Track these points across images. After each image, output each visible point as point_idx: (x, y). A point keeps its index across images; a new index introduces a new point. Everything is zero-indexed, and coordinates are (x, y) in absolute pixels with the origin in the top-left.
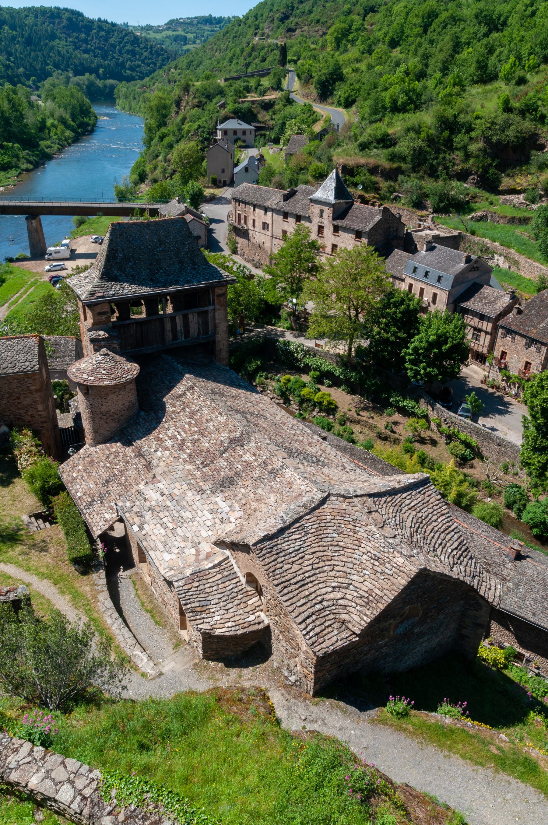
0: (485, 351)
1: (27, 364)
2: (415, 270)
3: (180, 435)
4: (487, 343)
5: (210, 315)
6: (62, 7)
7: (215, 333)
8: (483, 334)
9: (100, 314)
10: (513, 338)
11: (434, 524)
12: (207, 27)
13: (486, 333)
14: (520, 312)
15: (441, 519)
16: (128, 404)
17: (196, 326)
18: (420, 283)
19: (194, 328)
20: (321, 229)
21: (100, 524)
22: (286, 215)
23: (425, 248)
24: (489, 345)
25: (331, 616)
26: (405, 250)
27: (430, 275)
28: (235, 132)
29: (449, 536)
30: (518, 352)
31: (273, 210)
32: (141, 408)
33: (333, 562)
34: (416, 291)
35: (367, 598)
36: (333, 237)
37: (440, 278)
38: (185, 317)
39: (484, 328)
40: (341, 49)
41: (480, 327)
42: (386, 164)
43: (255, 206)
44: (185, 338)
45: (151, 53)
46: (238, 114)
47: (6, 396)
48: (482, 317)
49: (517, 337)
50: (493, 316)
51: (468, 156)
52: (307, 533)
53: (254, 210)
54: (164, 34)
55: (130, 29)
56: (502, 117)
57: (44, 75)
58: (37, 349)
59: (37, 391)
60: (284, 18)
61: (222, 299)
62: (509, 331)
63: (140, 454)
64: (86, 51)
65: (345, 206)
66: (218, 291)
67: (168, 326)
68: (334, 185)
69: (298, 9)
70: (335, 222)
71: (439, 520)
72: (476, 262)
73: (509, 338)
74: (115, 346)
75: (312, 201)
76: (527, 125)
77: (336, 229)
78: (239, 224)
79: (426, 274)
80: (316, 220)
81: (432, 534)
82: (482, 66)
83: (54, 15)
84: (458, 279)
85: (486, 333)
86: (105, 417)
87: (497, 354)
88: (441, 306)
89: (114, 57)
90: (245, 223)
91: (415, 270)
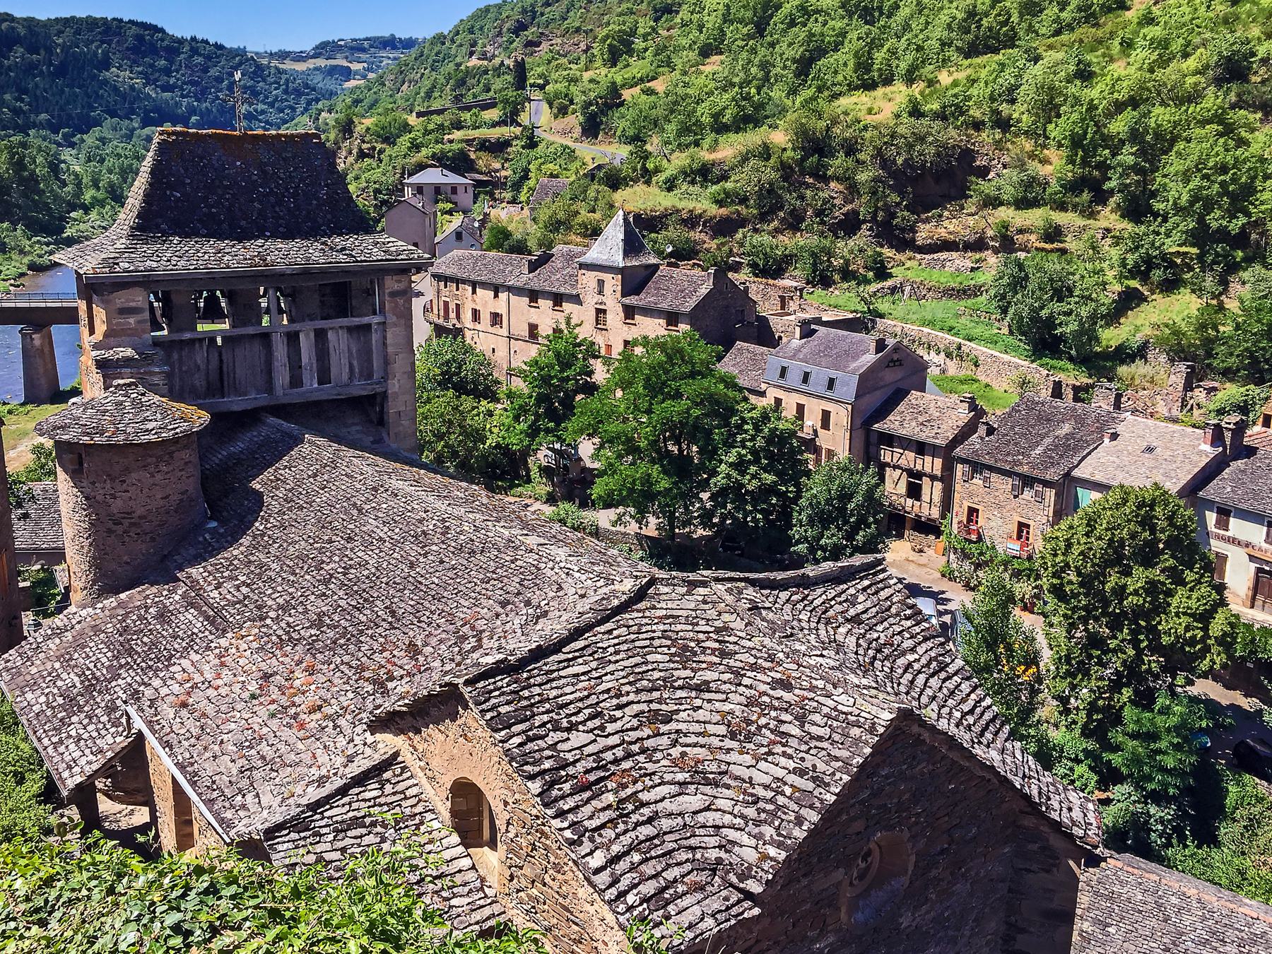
0: (935, 513)
5: (375, 337)
6: (126, 19)
7: (385, 378)
11: (911, 657)
13: (933, 478)
14: (991, 430)
15: (924, 646)
17: (345, 361)
18: (794, 395)
19: (340, 367)
20: (601, 313)
21: (83, 761)
22: (534, 296)
23: (798, 335)
24: (942, 502)
25: (683, 856)
28: (437, 189)
29: (950, 684)
31: (510, 289)
33: (673, 726)
34: (789, 412)
35: (771, 801)
36: (626, 328)
37: (831, 383)
38: (320, 335)
39: (928, 469)
40: (620, 65)
41: (919, 467)
42: (713, 210)
43: (474, 285)
45: (286, 92)
46: (441, 161)
48: (921, 448)
49: (995, 477)
51: (853, 189)
52: (603, 662)
53: (474, 292)
54: (311, 64)
55: (249, 55)
56: (906, 127)
57: (86, 125)
60: (520, 28)
62: (977, 467)
64: (167, 88)
65: (644, 273)
66: (392, 284)
67: (280, 350)
68: (622, 236)
69: (542, 14)
70: (627, 301)
71: (920, 650)
73: (977, 481)
74: (156, 380)
75: (583, 266)
76: (952, 135)
77: (630, 312)
78: (446, 317)
80: (591, 300)
81: (909, 676)
82: (864, 65)
83: (110, 29)
84: (867, 381)
85: (933, 478)
86: (119, 529)
88: (837, 441)
89: (217, 98)
90: (458, 317)
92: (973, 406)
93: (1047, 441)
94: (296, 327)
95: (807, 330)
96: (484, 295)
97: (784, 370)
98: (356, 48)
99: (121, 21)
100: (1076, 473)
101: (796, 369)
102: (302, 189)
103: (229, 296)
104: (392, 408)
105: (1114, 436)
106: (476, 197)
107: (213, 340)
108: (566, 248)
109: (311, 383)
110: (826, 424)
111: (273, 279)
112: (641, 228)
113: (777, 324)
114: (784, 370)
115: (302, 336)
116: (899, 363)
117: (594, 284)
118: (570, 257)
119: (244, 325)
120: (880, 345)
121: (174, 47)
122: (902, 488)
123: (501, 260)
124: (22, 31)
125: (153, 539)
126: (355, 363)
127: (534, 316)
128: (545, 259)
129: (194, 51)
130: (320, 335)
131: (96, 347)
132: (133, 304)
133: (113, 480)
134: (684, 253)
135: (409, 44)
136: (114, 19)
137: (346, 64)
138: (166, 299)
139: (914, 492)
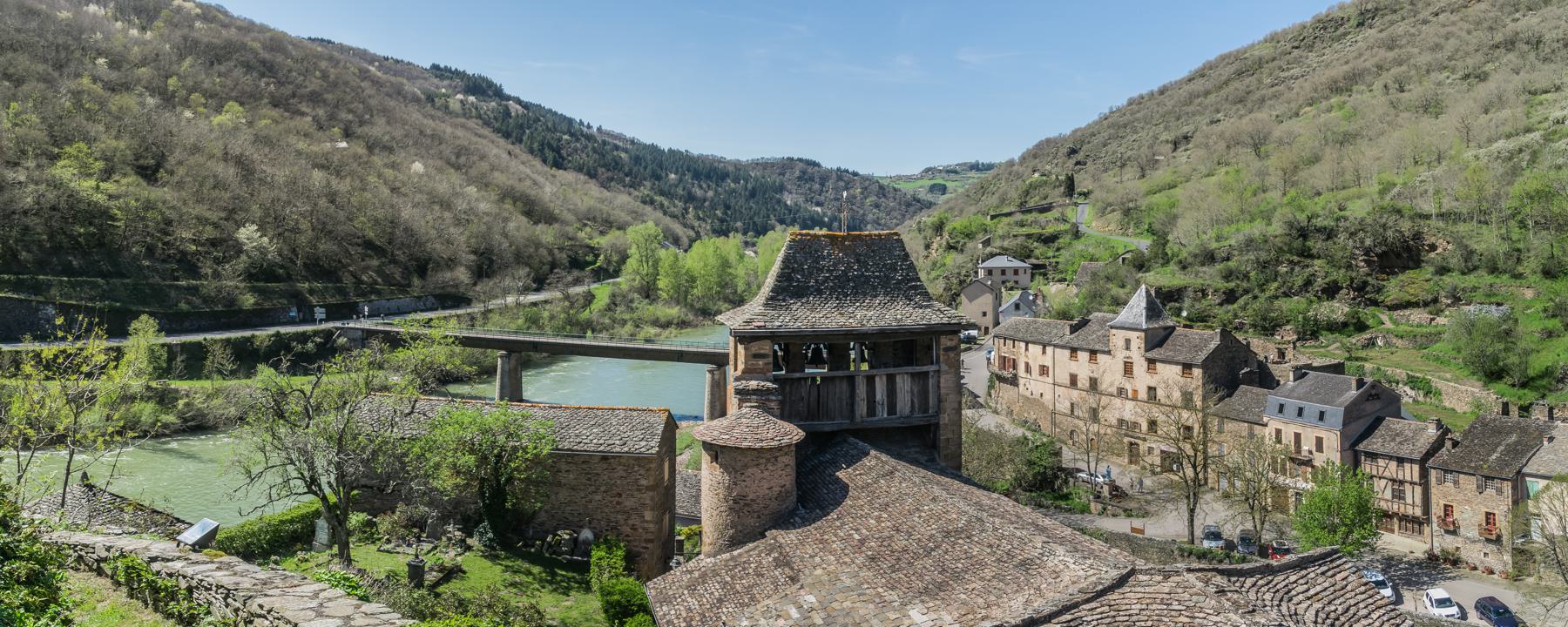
0: (1418, 512)
2: (1281, 408)
4: (1418, 500)
8: (1407, 486)
9: (756, 356)
10: (1456, 483)
12: (973, 174)
14: (1455, 444)
16: (777, 489)
17: (908, 397)
19: (904, 402)
20: (1128, 368)
26: (1261, 386)
27: (1305, 412)
28: (1003, 272)
30: (1469, 501)
38: (891, 379)
39: (1408, 478)
50: (1417, 456)
54: (920, 183)
58: (661, 428)
59: (648, 488)
61: (952, 355)
63: (783, 562)
65: (1163, 333)
66: (946, 341)
67: (861, 390)
70: (1149, 355)
72: (1373, 386)
74: (773, 405)
79: (1300, 412)
84: (1351, 414)
87: (1437, 510)
91: (1281, 408)
92: (1439, 425)
93: (1500, 449)
94: (874, 372)
95: (1300, 373)
96: (1035, 349)
97: (1282, 406)
98: (951, 171)
100: (1525, 470)
101: (1292, 404)
102: (879, 266)
103: (830, 348)
104: (944, 435)
105: (1551, 439)
106: (1033, 276)
107: (814, 379)
108: (1100, 315)
109: (882, 413)
110: (1319, 447)
111: (860, 336)
112: (1162, 300)
113: (1276, 370)
114: (1282, 406)
116: (1377, 397)
117: (1121, 343)
118: (1103, 322)
119: (837, 369)
120: (1360, 383)
121: (825, 177)
122: (1388, 494)
123: (1049, 325)
124: (731, 169)
127: (1074, 367)
128: (1084, 323)
129: (840, 178)
130: (891, 379)
131: (737, 379)
134: (1201, 319)
135: (990, 167)
138: (786, 350)
139: (1399, 495)
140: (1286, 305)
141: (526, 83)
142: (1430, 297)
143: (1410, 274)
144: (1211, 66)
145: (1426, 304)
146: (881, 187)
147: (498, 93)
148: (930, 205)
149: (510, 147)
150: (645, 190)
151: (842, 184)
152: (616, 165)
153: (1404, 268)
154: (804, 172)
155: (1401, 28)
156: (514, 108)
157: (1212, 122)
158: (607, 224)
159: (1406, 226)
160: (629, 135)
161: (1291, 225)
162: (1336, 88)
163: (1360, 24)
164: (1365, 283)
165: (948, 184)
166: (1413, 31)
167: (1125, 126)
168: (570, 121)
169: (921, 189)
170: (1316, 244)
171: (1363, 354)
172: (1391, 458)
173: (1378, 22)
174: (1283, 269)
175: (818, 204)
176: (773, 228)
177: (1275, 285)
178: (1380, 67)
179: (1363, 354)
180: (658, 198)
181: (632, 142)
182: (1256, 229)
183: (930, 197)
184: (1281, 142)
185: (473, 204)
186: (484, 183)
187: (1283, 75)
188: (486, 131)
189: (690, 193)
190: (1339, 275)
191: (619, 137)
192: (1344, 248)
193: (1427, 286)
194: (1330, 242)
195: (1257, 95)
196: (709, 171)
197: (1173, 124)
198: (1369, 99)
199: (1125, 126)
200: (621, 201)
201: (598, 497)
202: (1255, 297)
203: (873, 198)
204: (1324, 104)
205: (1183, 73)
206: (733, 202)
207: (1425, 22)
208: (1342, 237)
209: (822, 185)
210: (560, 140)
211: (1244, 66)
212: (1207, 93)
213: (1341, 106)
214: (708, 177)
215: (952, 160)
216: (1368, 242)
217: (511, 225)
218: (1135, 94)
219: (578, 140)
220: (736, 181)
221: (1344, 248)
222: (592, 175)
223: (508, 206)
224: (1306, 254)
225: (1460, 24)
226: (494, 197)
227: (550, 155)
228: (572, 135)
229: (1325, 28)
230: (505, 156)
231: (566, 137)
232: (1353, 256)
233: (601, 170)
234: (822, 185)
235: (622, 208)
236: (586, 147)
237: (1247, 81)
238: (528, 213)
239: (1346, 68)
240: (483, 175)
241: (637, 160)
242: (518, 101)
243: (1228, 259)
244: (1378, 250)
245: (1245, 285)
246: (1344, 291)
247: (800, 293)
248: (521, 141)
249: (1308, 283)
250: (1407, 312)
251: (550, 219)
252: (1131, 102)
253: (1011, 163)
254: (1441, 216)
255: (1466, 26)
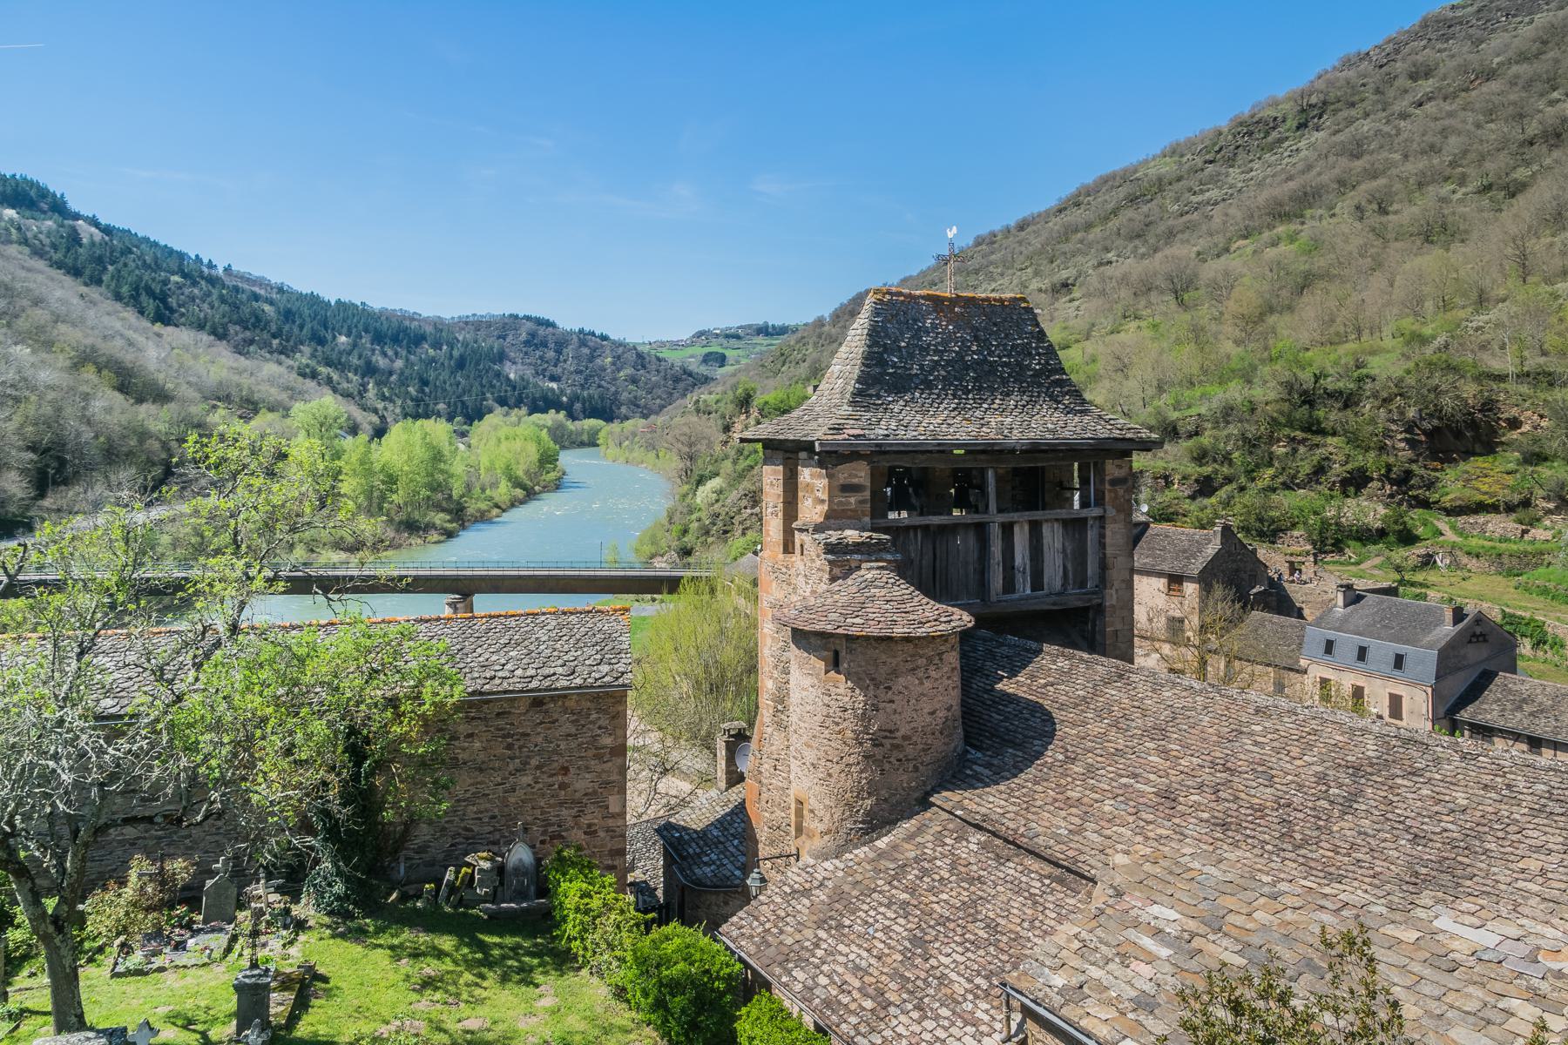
1: (605, 668)
3: (1148, 782)
5: (1091, 535)
6: (521, 315)
7: (1103, 581)
9: (848, 488)
12: (760, 339)
17: (1059, 562)
32: (968, 739)
38: (1035, 527)
44: (1033, 590)
47: (534, 762)
54: (690, 351)
67: (996, 549)
84: (1448, 660)
99: (516, 317)
109: (1024, 587)
115: (1016, 529)
121: (561, 343)
124: (429, 329)
125: (916, 769)
126: (1069, 567)
129: (583, 343)
130: (1035, 527)
132: (855, 481)
133: (877, 686)
135: (782, 331)
136: (511, 316)
137: (720, 350)
140: (1288, 501)
141: (104, 196)
142: (1516, 498)
143: (1477, 464)
144: (1089, 191)
145: (1510, 508)
146: (640, 356)
147: (58, 207)
148: (706, 380)
149: (84, 289)
150: (303, 357)
151: (586, 351)
152: (258, 321)
153: (1468, 454)
154: (533, 335)
155: (1366, 126)
156: (87, 232)
157: (1100, 264)
158: (250, 407)
159: (1469, 390)
160: (275, 279)
161: (1289, 386)
162: (1280, 213)
163: (1302, 126)
164: (1408, 474)
165: (728, 353)
166: (1387, 129)
167: (977, 272)
168: (181, 256)
169: (691, 358)
170: (1330, 415)
171: (1419, 577)
172: (1517, 737)
173: (1327, 120)
174: (1280, 450)
175: (553, 378)
176: (490, 411)
177: (1271, 471)
178: (1341, 183)
179: (1419, 577)
180: (323, 370)
181: (281, 290)
182: (1235, 392)
183: (703, 370)
184: (1214, 286)
185: (29, 373)
186: (42, 341)
187: (1195, 199)
188: (40, 264)
189: (368, 363)
190: (1369, 460)
191: (259, 282)
192: (1373, 421)
193: (1510, 480)
194: (1349, 412)
195: (1161, 228)
196: (399, 333)
197: (1045, 267)
198: (1338, 225)
199: (977, 272)
200: (267, 373)
201: (526, 779)
202: (1242, 489)
203: (629, 371)
204: (1266, 235)
205: (1051, 202)
206: (432, 375)
207: (1404, 116)
208: (1367, 407)
209: (559, 352)
210: (166, 282)
211: (1137, 190)
212: (1089, 226)
213: (1292, 239)
214: (396, 340)
215: (732, 322)
216: (1411, 413)
217: (97, 406)
218: (984, 231)
219: (195, 284)
220: (437, 345)
221: (1373, 421)
222: (220, 334)
223: (89, 373)
224: (1315, 428)
225: (1462, 114)
226: (62, 361)
227: (150, 305)
228: (185, 276)
229: (1250, 134)
230: (76, 300)
231: (176, 278)
232: (1387, 434)
233: (232, 329)
234: (559, 352)
235: (271, 381)
236: (209, 294)
237: (1145, 208)
238: (122, 388)
239: (1291, 184)
240: (40, 329)
241: (288, 315)
242: (94, 222)
243: (1196, 433)
244: (1426, 425)
245: (1225, 470)
246: (1375, 484)
247: (900, 385)
248: (99, 282)
249: (1320, 470)
250: (1481, 519)
251: (162, 397)
252: (979, 242)
253: (820, 323)
254: (1523, 376)
255: (1470, 117)
